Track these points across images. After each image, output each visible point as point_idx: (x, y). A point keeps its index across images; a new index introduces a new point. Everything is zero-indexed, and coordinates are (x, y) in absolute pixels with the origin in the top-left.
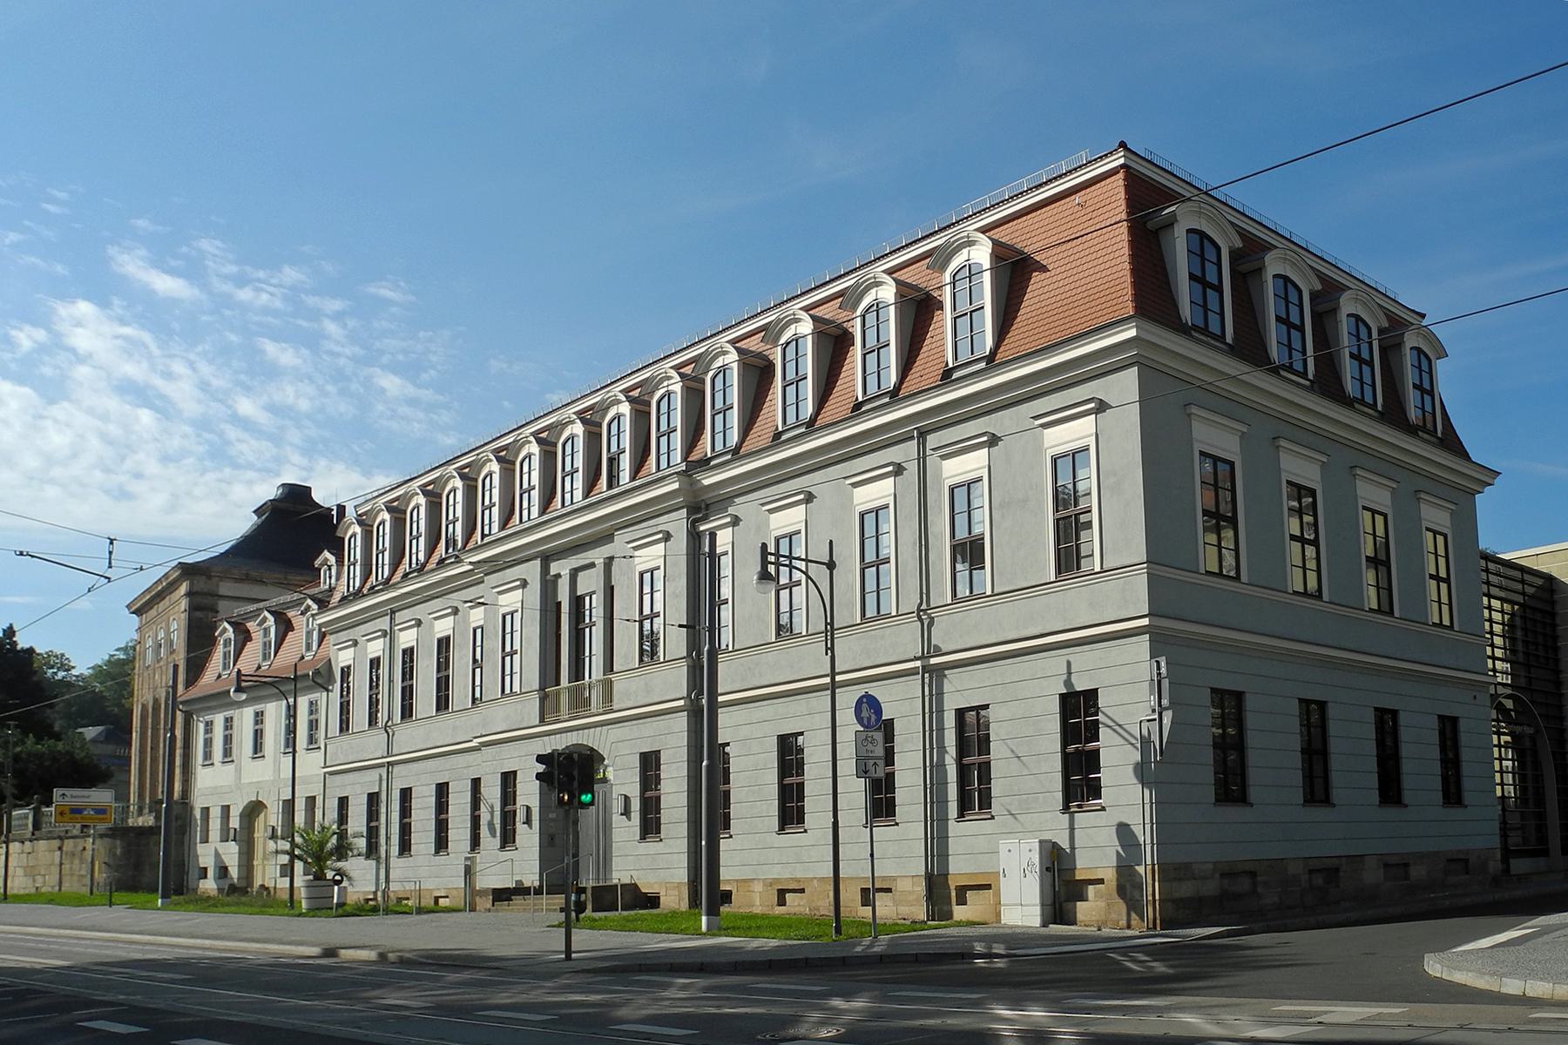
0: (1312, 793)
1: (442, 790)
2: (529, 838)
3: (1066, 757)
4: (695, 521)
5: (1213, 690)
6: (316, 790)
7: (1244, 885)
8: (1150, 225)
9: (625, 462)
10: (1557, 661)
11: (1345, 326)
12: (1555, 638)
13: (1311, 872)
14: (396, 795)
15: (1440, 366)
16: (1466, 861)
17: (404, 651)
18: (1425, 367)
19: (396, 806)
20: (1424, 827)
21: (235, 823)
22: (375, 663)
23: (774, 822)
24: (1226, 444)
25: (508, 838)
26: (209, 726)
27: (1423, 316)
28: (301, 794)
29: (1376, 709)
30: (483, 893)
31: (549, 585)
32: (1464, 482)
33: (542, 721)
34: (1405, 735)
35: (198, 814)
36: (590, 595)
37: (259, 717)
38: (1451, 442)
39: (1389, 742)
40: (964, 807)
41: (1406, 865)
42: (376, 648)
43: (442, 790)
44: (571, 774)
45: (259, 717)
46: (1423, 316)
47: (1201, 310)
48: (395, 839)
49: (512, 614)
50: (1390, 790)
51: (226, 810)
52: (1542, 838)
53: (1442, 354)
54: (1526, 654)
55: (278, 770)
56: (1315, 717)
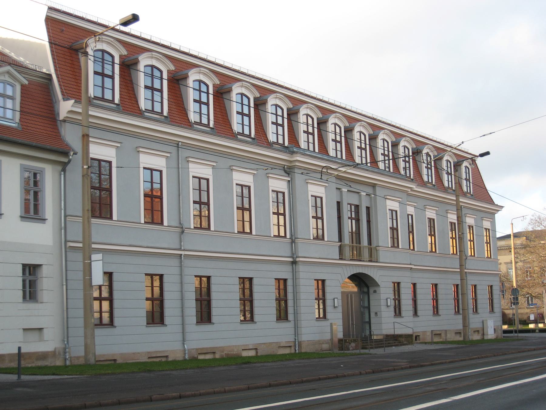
0: (280, 317)
38: (490, 201)
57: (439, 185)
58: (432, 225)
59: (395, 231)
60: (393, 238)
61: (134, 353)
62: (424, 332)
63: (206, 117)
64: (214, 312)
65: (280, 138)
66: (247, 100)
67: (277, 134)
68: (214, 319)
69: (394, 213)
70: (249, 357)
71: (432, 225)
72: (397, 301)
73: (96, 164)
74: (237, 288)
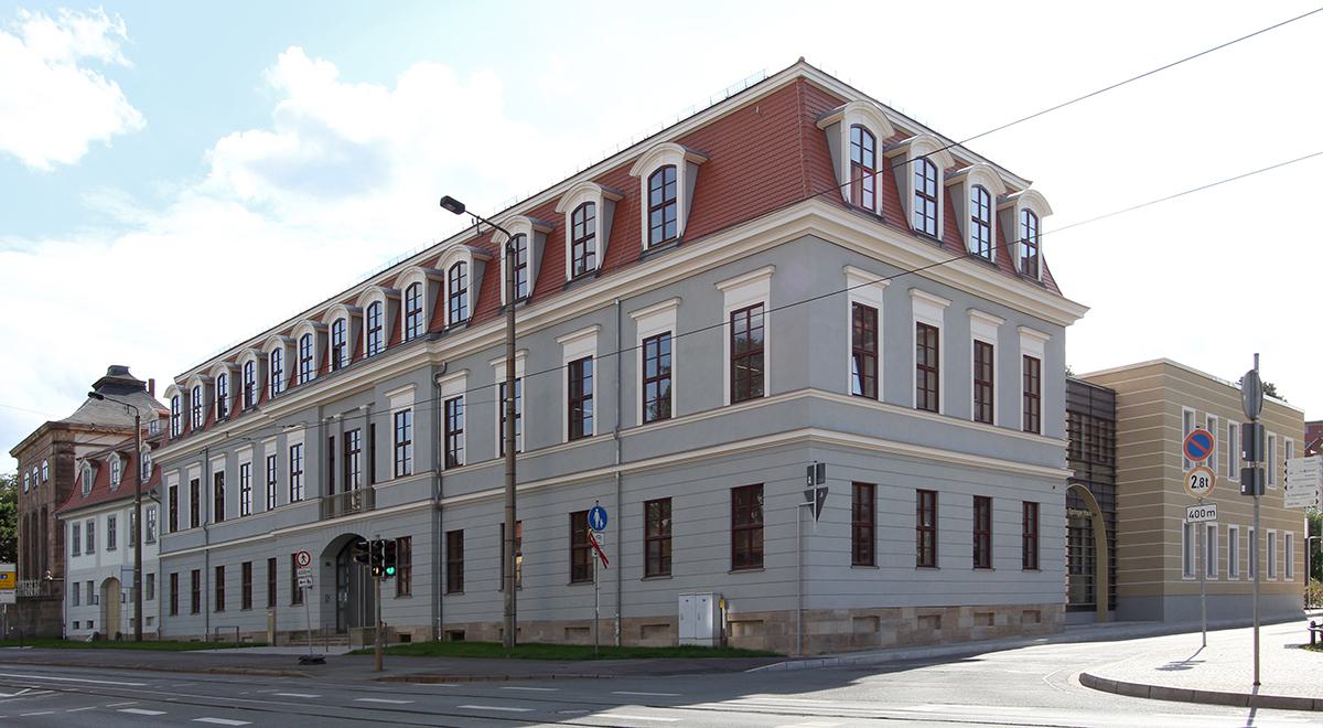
0: (922, 561)
1: (247, 567)
2: (313, 599)
3: (734, 532)
4: (438, 376)
5: (854, 483)
6: (155, 570)
7: (867, 627)
8: (820, 125)
9: (346, 352)
10: (1114, 460)
11: (972, 194)
12: (1114, 441)
13: (920, 617)
14: (213, 571)
15: (1046, 224)
16: (1038, 613)
17: (171, 488)
18: (1032, 225)
19: (213, 579)
20: (1007, 582)
21: (97, 592)
22: (195, 483)
23: (728, 563)
24: (872, 296)
25: (297, 597)
26: (77, 528)
27: (1030, 183)
28: (145, 572)
29: (975, 497)
30: (282, 633)
31: (323, 426)
32: (1056, 318)
33: (322, 519)
34: (996, 516)
35: (70, 588)
36: (356, 431)
37: (112, 523)
38: (1047, 284)
39: (865, 531)
40: (450, 591)
41: (992, 614)
42: (195, 473)
43: (247, 567)
44: (349, 553)
45: (112, 523)
46: (1030, 183)
47: (922, 178)
48: (213, 601)
49: (298, 446)
50: (982, 557)
51: (91, 583)
52: (1091, 597)
53: (1048, 211)
54: (1089, 454)
55: (126, 558)
56: (927, 504)
57: (954, 238)
58: (1034, 374)
59: (1034, 401)
60: (1028, 413)
61: (192, 641)
62: (475, 626)
63: (933, 221)
64: (941, 549)
65: (930, 223)
66: (933, 170)
67: (925, 215)
68: (995, 562)
69: (1034, 364)
70: (658, 648)
71: (1034, 374)
72: (1030, 540)
73: (636, 228)
74: (970, 513)
